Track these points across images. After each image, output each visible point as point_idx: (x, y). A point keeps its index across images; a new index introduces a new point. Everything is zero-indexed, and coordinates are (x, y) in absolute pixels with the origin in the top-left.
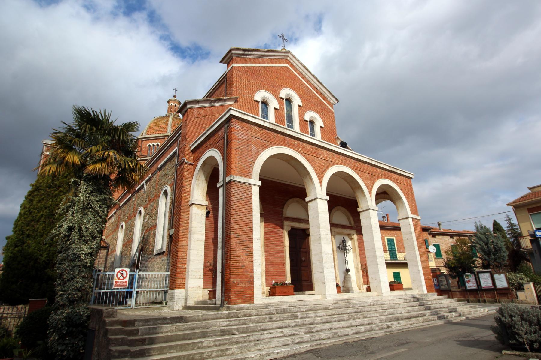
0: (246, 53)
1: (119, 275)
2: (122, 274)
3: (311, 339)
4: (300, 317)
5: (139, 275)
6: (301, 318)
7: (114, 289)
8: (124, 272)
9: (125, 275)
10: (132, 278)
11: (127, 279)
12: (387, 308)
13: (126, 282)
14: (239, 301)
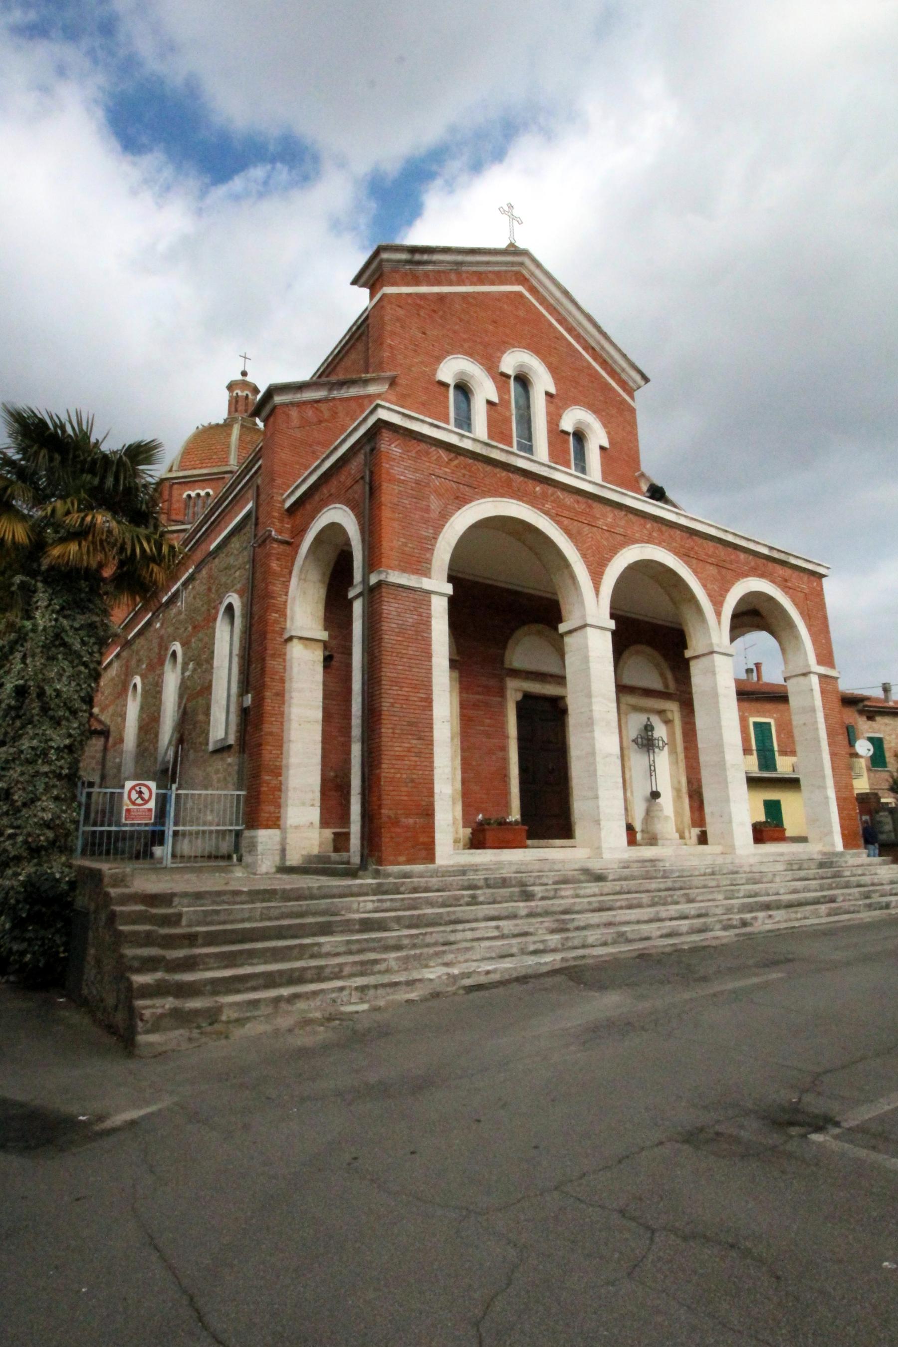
0: (417, 257)
1: (134, 795)
2: (140, 793)
3: (563, 945)
4: (540, 895)
5: (178, 796)
6: (543, 898)
7: (126, 825)
8: (144, 789)
9: (146, 796)
10: (162, 801)
11: (152, 805)
12: (744, 881)
13: (150, 810)
14: (402, 859)
